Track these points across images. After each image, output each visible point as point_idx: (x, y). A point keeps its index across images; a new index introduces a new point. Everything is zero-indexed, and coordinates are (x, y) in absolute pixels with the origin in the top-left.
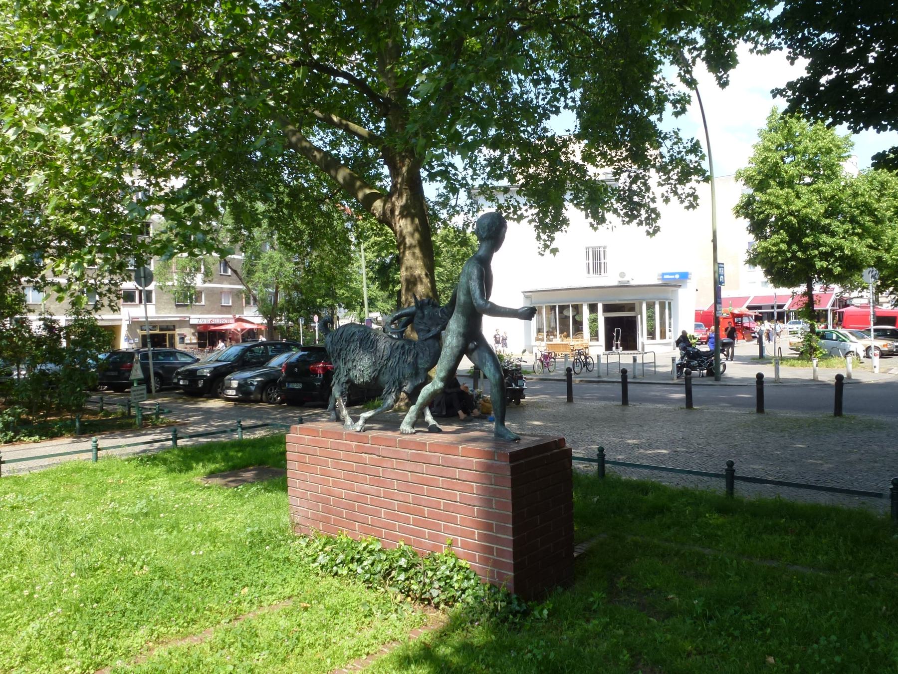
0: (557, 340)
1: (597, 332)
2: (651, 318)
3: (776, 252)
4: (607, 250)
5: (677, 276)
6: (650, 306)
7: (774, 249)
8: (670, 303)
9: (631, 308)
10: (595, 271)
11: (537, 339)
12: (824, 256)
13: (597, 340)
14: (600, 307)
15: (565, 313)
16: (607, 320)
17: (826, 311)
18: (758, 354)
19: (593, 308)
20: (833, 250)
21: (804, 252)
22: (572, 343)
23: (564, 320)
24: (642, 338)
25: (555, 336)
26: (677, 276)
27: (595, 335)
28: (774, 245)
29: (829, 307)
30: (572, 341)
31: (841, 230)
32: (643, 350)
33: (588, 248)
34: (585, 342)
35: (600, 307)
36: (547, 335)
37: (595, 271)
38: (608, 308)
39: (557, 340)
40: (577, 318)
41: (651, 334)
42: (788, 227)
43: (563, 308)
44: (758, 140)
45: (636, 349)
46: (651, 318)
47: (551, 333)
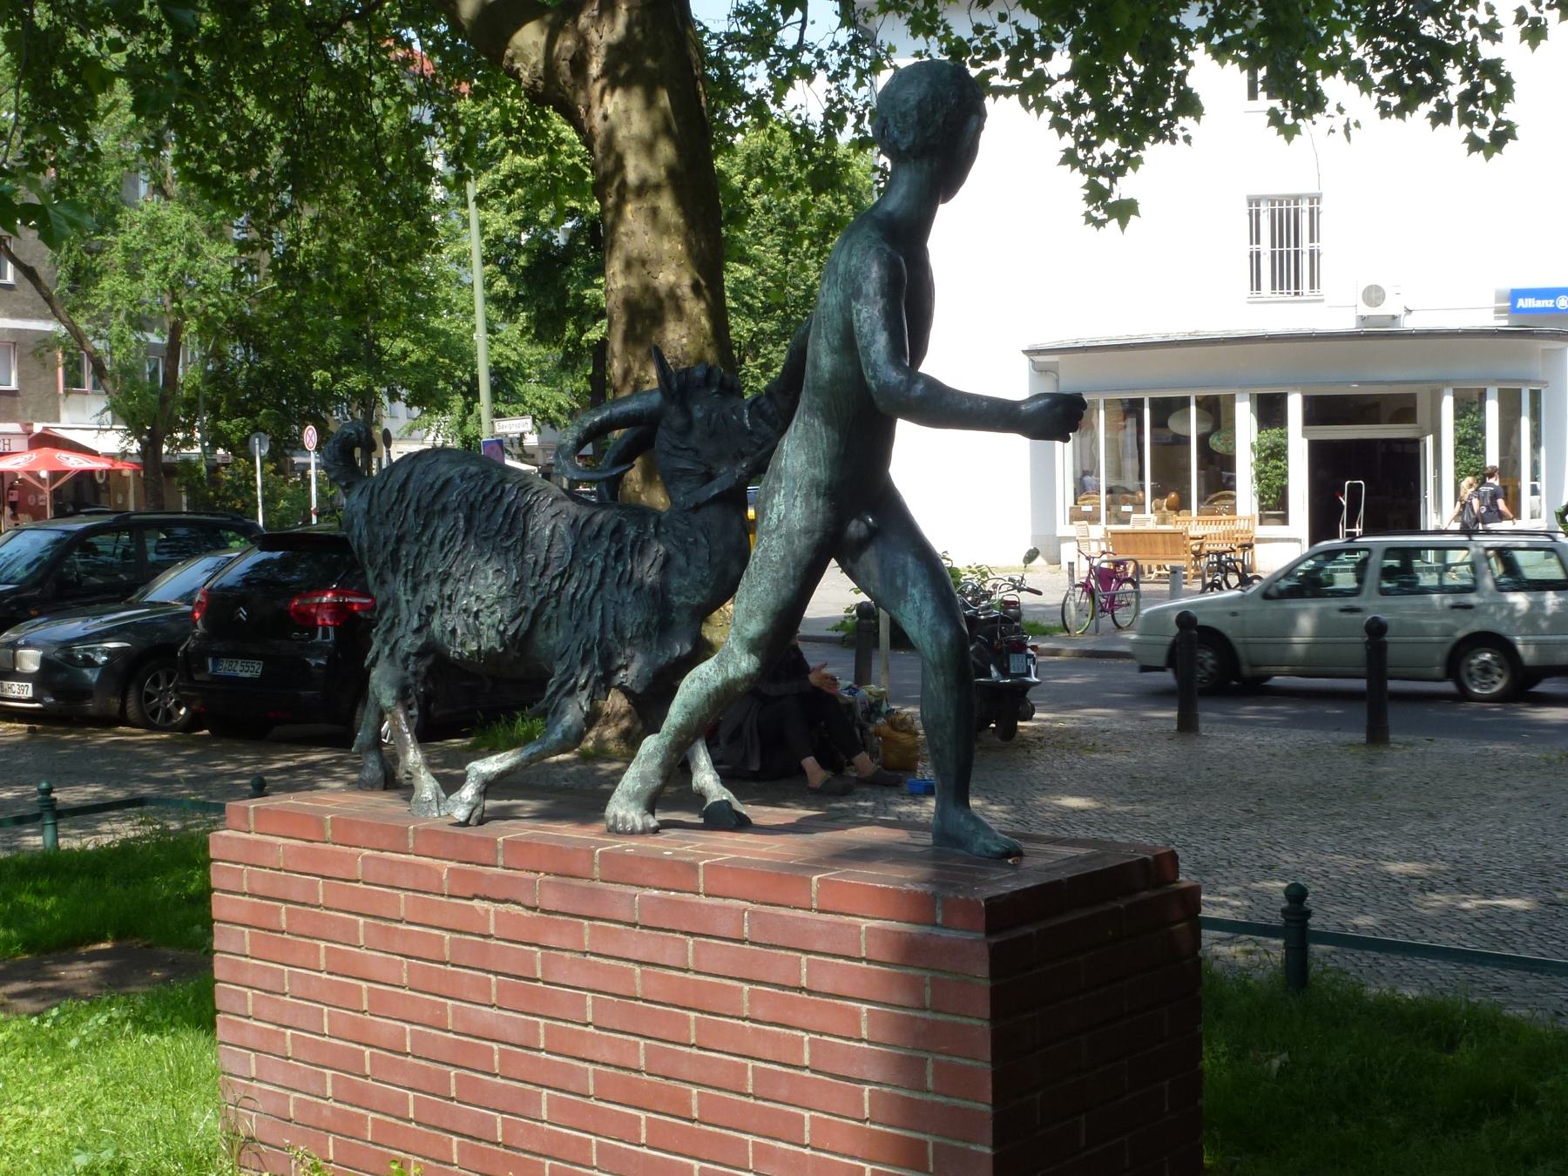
1: (1283, 493)
6: (1469, 407)
9: (1403, 408)
13: (1284, 520)
14: (1295, 406)
15: (1174, 425)
16: (1319, 452)
19: (1270, 411)
22: (1196, 530)
23: (1170, 450)
25: (1139, 507)
27: (1274, 504)
30: (1196, 525)
33: (1254, 201)
34: (1241, 525)
35: (1295, 406)
38: (1320, 410)
40: (1215, 443)
43: (1166, 409)
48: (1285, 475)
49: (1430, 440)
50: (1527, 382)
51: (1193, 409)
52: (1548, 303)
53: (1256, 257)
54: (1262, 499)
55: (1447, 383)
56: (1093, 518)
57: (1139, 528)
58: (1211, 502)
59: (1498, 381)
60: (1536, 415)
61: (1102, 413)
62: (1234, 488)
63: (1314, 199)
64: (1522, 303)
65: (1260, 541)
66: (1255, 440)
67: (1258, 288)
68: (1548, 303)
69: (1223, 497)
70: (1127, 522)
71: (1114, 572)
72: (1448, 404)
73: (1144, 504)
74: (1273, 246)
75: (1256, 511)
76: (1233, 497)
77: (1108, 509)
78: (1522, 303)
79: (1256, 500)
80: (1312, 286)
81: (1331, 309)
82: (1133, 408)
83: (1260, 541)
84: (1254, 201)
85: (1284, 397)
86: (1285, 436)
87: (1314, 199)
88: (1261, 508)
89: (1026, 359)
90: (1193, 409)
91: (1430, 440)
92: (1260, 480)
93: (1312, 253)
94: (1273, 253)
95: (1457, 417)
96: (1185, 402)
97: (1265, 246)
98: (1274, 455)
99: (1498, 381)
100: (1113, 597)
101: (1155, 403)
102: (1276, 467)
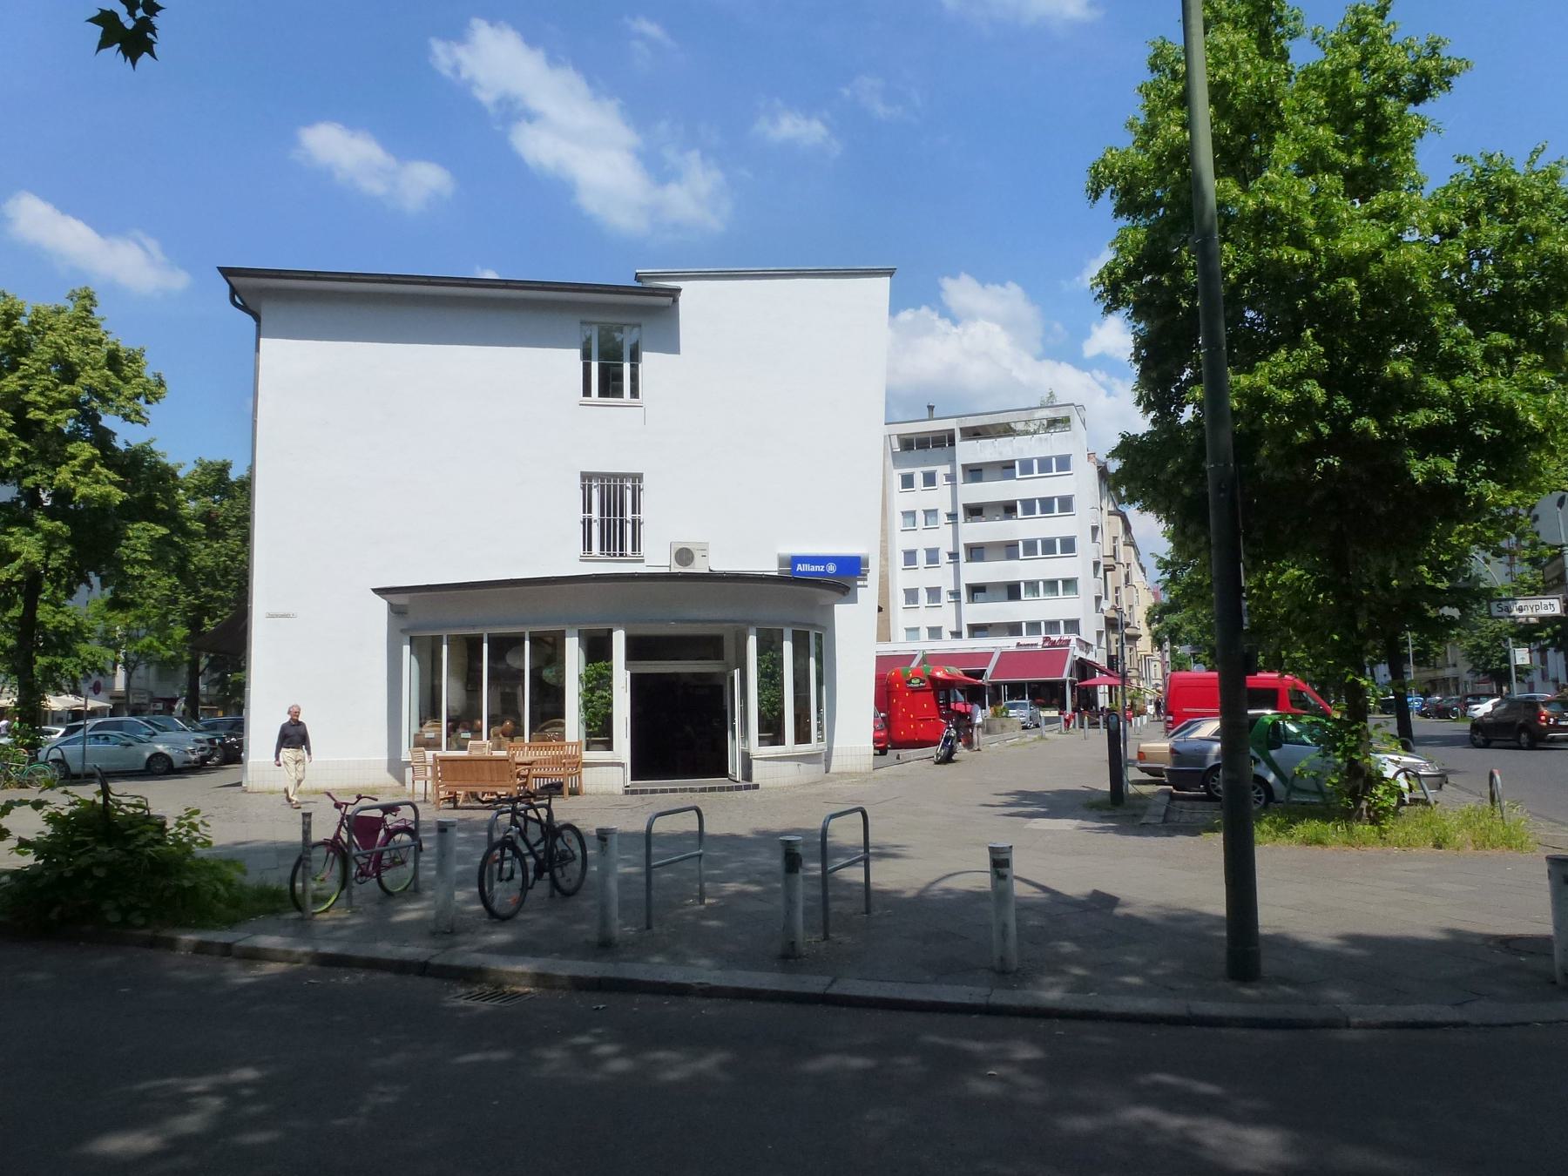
0: (483, 746)
1: (608, 719)
2: (770, 677)
3: (1291, 410)
4: (645, 484)
5: (832, 568)
6: (769, 647)
7: (1287, 396)
8: (819, 637)
9: (710, 646)
10: (604, 392)
11: (421, 743)
12: (1432, 440)
13: (608, 746)
14: (619, 640)
15: (511, 660)
16: (639, 685)
17: (1064, 683)
18: (1105, 786)
19: (597, 649)
20: (1465, 420)
21: (1381, 417)
22: (523, 756)
23: (506, 679)
24: (746, 740)
25: (477, 733)
26: (832, 568)
27: (599, 732)
28: (1281, 383)
29: (1065, 676)
30: (526, 751)
31: (1476, 351)
32: (747, 775)
33: (586, 477)
34: (570, 750)
35: (619, 640)
36: (452, 730)
37: (604, 392)
38: (636, 649)
39: (483, 746)
40: (548, 674)
41: (772, 730)
42: (1330, 318)
43: (505, 646)
44: (1149, 77)
45: (723, 771)
46: (770, 677)
47: (464, 721)
48: (610, 704)
49: (737, 672)
50: (814, 626)
51: (527, 643)
52: (821, 569)
53: (587, 524)
54: (588, 726)
55: (751, 623)
56: (434, 744)
57: (476, 754)
58: (542, 730)
59: (794, 623)
60: (819, 661)
61: (445, 647)
62: (563, 716)
63: (637, 478)
64: (799, 567)
65: (586, 765)
66: (582, 672)
67: (590, 549)
68: (821, 569)
69: (553, 725)
70: (465, 748)
71: (383, 820)
72: (752, 643)
73: (481, 731)
74: (602, 514)
75: (583, 738)
76: (563, 725)
77: (448, 736)
78: (799, 567)
79: (583, 728)
80: (634, 549)
81: (655, 557)
82: (473, 644)
83: (586, 765)
84: (586, 477)
85: (610, 632)
86: (610, 669)
87: (637, 478)
88: (588, 735)
89: (382, 604)
90: (527, 643)
91: (737, 672)
92: (586, 709)
93: (634, 521)
94: (602, 521)
95: (759, 653)
96: (517, 641)
97: (595, 515)
98: (597, 684)
99: (794, 623)
100: (380, 855)
101: (493, 641)
102: (602, 697)
